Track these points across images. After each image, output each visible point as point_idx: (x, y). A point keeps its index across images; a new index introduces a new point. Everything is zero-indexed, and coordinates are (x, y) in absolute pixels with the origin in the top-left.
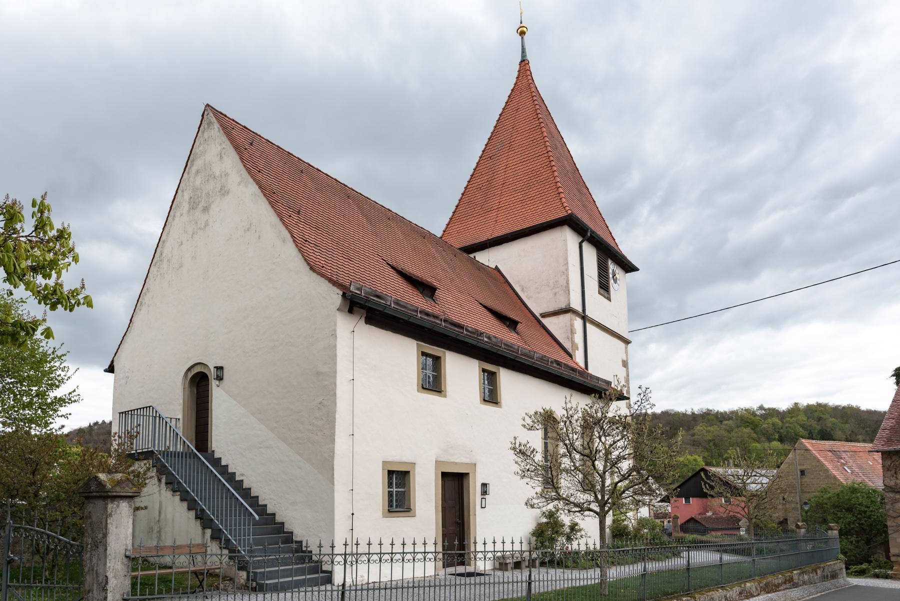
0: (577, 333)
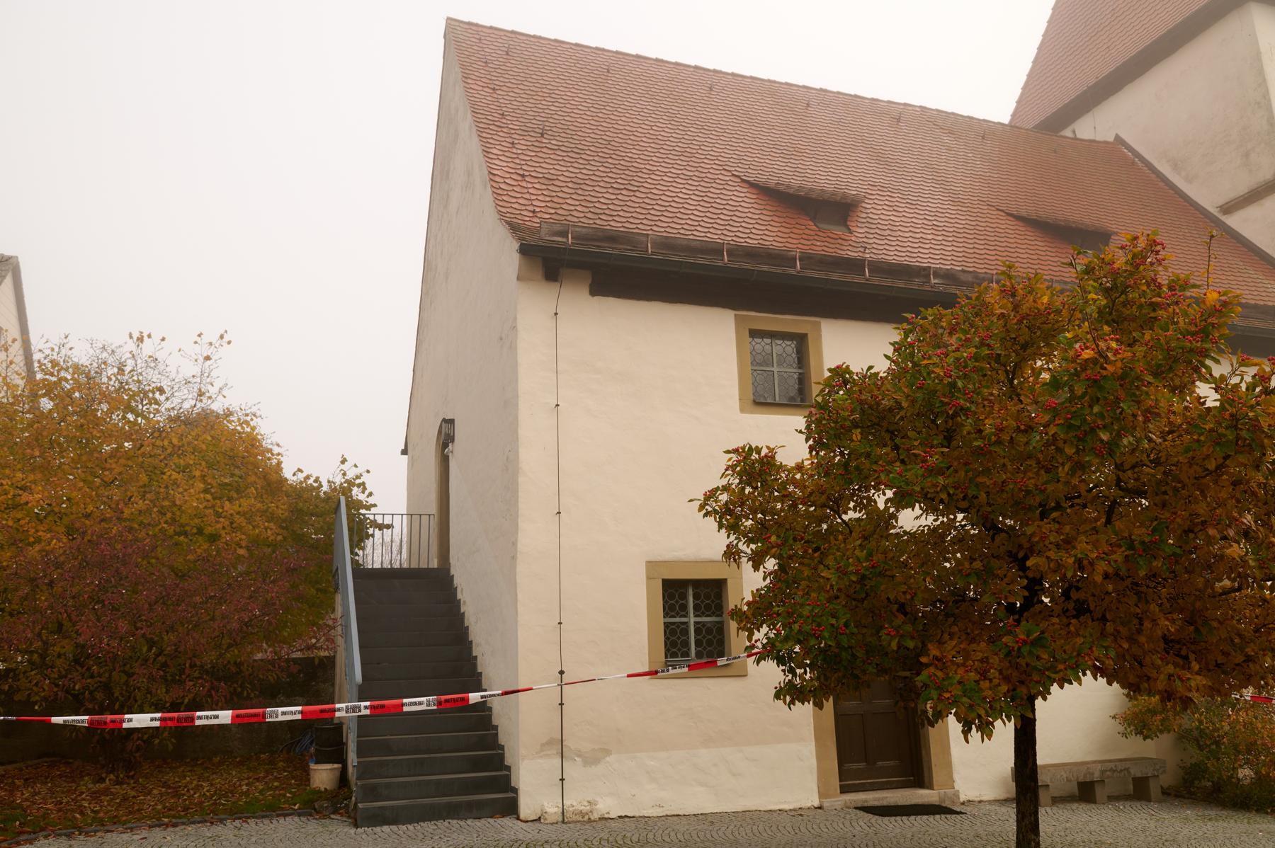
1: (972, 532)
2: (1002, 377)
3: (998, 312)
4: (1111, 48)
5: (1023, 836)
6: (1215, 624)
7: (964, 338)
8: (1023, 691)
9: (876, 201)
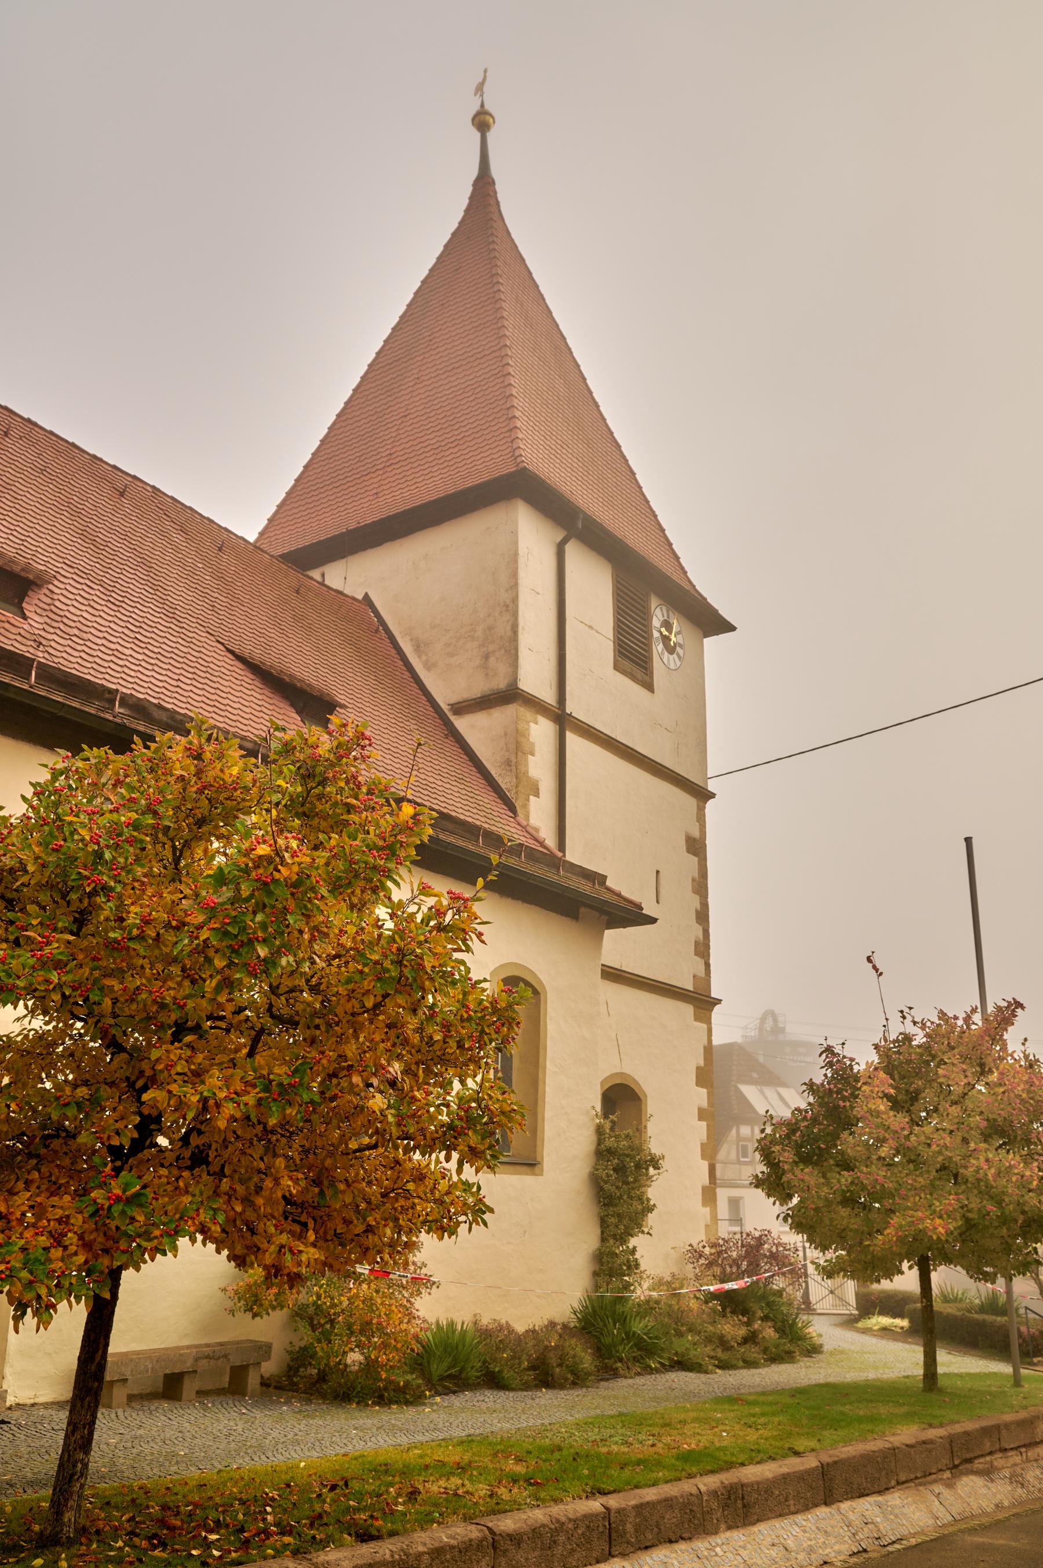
0: (536, 754)
1: (92, 1044)
2: (168, 853)
3: (178, 772)
4: (380, 495)
5: (69, 1456)
6: (342, 1187)
7: (128, 797)
8: (105, 1262)
9: (68, 587)
